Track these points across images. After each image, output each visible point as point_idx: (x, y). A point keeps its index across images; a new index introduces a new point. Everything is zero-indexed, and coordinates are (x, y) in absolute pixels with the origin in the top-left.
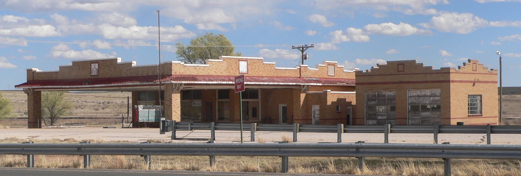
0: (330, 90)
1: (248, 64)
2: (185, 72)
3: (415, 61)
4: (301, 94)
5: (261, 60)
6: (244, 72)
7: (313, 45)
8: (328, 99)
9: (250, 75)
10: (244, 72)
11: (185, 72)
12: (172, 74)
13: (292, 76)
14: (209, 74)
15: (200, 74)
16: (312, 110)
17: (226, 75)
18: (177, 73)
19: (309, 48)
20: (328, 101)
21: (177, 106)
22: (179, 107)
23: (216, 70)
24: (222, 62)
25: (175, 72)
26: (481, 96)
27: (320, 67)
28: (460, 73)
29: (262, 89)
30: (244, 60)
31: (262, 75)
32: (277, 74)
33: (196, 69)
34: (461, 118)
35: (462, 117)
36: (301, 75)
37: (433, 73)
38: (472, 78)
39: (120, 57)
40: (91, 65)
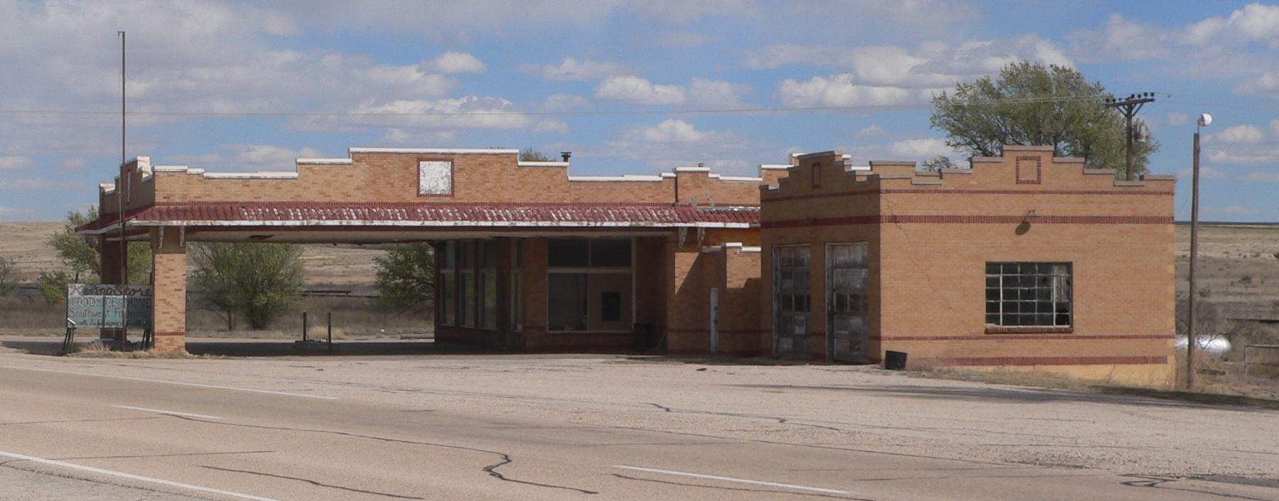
0: (740, 244)
2: (208, 195)
3: (834, 155)
4: (677, 254)
6: (437, 191)
7: (1152, 94)
8: (728, 270)
10: (439, 193)
11: (208, 195)
12: (157, 200)
13: (644, 199)
14: (300, 200)
15: (262, 200)
16: (709, 303)
17: (366, 201)
18: (172, 198)
19: (1144, 104)
21: (173, 288)
22: (180, 290)
23: (325, 189)
24: (350, 164)
25: (166, 196)
26: (1068, 266)
27: (770, 172)
28: (939, 192)
29: (640, 239)
30: (438, 157)
31: (510, 199)
32: (577, 197)
33: (248, 186)
34: (946, 338)
36: (679, 197)
37: (855, 193)
38: (1016, 206)
39: (147, 156)
40: (418, 165)
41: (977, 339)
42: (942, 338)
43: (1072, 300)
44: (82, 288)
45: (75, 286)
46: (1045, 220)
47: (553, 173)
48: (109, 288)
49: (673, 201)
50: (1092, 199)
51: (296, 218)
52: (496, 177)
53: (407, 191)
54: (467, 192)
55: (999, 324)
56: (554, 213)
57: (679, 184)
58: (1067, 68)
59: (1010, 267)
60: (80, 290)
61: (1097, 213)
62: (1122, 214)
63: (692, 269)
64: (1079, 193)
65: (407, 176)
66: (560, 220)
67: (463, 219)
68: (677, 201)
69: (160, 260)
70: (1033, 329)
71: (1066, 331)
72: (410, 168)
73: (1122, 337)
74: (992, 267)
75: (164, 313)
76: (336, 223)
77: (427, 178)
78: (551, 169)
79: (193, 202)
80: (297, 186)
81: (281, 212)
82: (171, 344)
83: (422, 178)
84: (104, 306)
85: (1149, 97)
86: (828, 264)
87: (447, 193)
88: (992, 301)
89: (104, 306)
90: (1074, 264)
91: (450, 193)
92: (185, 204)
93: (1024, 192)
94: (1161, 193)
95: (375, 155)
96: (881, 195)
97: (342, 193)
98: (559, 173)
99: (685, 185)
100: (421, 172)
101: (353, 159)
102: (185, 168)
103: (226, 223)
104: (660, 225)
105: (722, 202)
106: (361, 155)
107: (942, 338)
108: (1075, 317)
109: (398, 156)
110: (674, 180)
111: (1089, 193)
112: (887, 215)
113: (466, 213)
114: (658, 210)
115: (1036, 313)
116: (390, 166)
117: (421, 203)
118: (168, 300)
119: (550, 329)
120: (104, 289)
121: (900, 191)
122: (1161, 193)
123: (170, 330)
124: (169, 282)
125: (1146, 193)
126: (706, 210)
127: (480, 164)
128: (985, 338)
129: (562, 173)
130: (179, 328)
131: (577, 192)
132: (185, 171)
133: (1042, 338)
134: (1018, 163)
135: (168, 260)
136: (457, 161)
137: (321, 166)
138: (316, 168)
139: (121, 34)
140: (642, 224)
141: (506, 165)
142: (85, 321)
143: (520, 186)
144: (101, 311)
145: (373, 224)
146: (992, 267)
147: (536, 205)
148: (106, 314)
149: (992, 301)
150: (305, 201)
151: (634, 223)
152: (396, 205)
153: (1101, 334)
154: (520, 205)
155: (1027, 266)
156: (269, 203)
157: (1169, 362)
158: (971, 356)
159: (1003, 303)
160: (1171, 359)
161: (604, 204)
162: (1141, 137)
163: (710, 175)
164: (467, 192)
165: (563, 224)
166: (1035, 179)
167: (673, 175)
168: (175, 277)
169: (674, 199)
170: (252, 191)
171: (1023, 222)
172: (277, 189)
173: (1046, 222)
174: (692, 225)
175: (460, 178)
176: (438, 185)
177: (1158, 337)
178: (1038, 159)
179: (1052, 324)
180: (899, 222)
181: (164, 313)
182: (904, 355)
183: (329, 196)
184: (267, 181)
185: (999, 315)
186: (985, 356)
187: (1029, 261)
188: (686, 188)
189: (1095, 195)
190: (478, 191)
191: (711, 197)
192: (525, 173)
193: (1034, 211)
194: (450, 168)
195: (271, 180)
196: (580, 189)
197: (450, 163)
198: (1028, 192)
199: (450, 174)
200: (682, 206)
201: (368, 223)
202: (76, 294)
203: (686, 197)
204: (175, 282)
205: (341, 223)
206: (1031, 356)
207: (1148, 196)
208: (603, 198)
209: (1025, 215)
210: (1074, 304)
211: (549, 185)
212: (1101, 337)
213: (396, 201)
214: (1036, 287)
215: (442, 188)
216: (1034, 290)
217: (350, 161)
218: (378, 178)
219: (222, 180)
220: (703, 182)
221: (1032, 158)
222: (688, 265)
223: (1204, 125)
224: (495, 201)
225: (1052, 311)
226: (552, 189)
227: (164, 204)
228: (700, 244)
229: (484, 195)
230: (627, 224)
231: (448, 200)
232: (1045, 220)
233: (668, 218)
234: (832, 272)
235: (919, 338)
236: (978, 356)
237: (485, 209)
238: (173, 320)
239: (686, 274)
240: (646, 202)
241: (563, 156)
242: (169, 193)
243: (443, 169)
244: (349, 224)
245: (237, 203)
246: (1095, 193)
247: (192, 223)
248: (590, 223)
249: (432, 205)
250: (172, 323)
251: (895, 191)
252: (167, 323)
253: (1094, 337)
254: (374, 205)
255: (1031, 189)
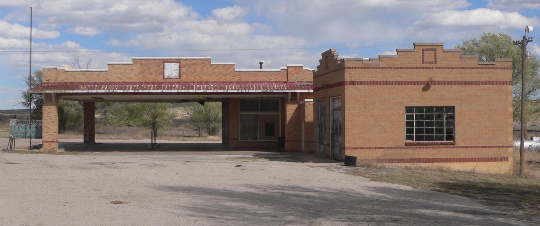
1: (181, 66)
2: (66, 79)
3: (331, 51)
4: (287, 105)
5: (206, 61)
6: (172, 76)
7: (532, 38)
8: (306, 112)
9: (183, 80)
10: (173, 77)
11: (67, 79)
13: (272, 80)
14: (108, 81)
17: (139, 81)
18: (50, 80)
20: (308, 115)
23: (120, 76)
24: (131, 64)
25: (47, 80)
26: (451, 109)
28: (378, 68)
30: (173, 61)
31: (207, 80)
32: (239, 79)
33: (85, 75)
34: (383, 148)
35: (383, 146)
36: (288, 78)
38: (423, 76)
40: (164, 65)
41: (400, 148)
42: (380, 148)
43: (455, 126)
44: (16, 121)
45: (13, 120)
46: (439, 83)
47: (228, 67)
48: (28, 121)
49: (286, 80)
50: (466, 72)
51: (104, 89)
52: (200, 70)
53: (158, 77)
54: (187, 76)
55: (413, 140)
56: (227, 86)
57: (288, 73)
58: (505, 34)
59: (420, 109)
60: (15, 122)
61: (469, 79)
62: (482, 80)
63: (294, 112)
64: (457, 68)
65: (158, 70)
66: (228, 89)
67: (182, 89)
68: (288, 80)
69: (45, 108)
70: (433, 143)
71: (451, 144)
72: (160, 66)
73: (483, 147)
74: (409, 109)
75: (46, 132)
76: (121, 91)
77: (168, 70)
78: (227, 66)
79: (60, 82)
80: (107, 75)
81: (98, 86)
82: (50, 146)
83: (165, 70)
84: (25, 129)
85: (530, 39)
86: (331, 109)
87: (177, 77)
88: (410, 128)
89: (25, 129)
90: (455, 107)
91: (179, 77)
92: (56, 83)
93: (427, 68)
94: (504, 68)
95: (143, 60)
96: (345, 70)
97: (128, 78)
98: (231, 67)
99: (292, 73)
100: (165, 68)
101: (133, 62)
102: (56, 67)
103: (70, 92)
104: (277, 91)
105: (310, 81)
106: (137, 60)
107: (380, 148)
108: (456, 136)
109: (154, 60)
110: (286, 70)
111: (464, 68)
112: (349, 81)
113: (184, 86)
114: (278, 84)
115: (435, 134)
116: (150, 65)
117: (165, 82)
118: (48, 127)
119: (241, 139)
120: (25, 121)
121: (356, 68)
122: (504, 68)
123: (49, 140)
124: (49, 119)
125: (496, 68)
126: (301, 84)
127: (193, 64)
128: (405, 148)
129: (232, 67)
130: (53, 139)
131: (239, 76)
132: (56, 68)
133: (438, 148)
134: (424, 52)
135: (49, 109)
136: (183, 63)
137: (118, 65)
138: (116, 66)
139: (30, 8)
140: (268, 91)
141: (205, 64)
142: (17, 136)
143: (212, 74)
144: (24, 131)
145: (139, 92)
146: (409, 109)
147: (219, 82)
148: (27, 132)
149: (410, 128)
150: (111, 81)
151: (264, 91)
152: (153, 83)
153: (471, 145)
154: (212, 83)
155: (430, 109)
156: (94, 82)
157: (509, 160)
158: (397, 158)
159: (416, 129)
160: (511, 159)
161: (253, 82)
162: (528, 57)
163: (304, 68)
164: (187, 76)
165: (229, 91)
166: (434, 61)
167: (286, 68)
168: (52, 116)
169: (286, 79)
170: (87, 77)
171: (427, 85)
172: (98, 76)
173: (439, 84)
174: (293, 91)
175: (184, 70)
176: (173, 74)
177: (503, 147)
178: (435, 50)
179: (444, 140)
180: (355, 85)
181: (46, 132)
182: (355, 158)
183: (122, 79)
184: (93, 72)
185: (414, 135)
186: (405, 158)
187: (430, 105)
188: (292, 74)
189: (468, 70)
190: (191, 77)
191: (304, 78)
192: (214, 68)
193: (432, 78)
194: (179, 66)
195: (95, 72)
196: (241, 75)
197: (179, 63)
198: (429, 68)
199: (179, 69)
200: (290, 82)
201: (136, 91)
202: (13, 124)
203: (292, 78)
204: (51, 119)
205: (124, 91)
206: (432, 158)
207: (497, 70)
208: (252, 79)
209: (428, 80)
210: (456, 129)
211: (226, 73)
212: (471, 147)
213: (153, 81)
214: (435, 120)
215: (175, 75)
216: (434, 121)
217: (131, 63)
218: (145, 71)
219: (73, 72)
220: (300, 71)
221: (432, 50)
222: (293, 110)
223: (529, 32)
224: (200, 81)
225: (444, 133)
226: (227, 75)
227: (46, 83)
228: (298, 101)
229: (195, 78)
230: (261, 91)
231: (178, 80)
232: (439, 83)
233: (281, 88)
234: (334, 112)
235: (367, 148)
236: (401, 158)
237: (195, 84)
238: (51, 135)
239: (292, 115)
240: (272, 81)
241: (260, 64)
242: (49, 78)
243: (176, 66)
244: (127, 92)
245: (80, 83)
246: (467, 68)
247: (59, 92)
248: (243, 91)
249: (170, 83)
250: (50, 137)
251: (353, 68)
252: (48, 137)
253: (467, 147)
254: (142, 83)
255: (431, 66)
